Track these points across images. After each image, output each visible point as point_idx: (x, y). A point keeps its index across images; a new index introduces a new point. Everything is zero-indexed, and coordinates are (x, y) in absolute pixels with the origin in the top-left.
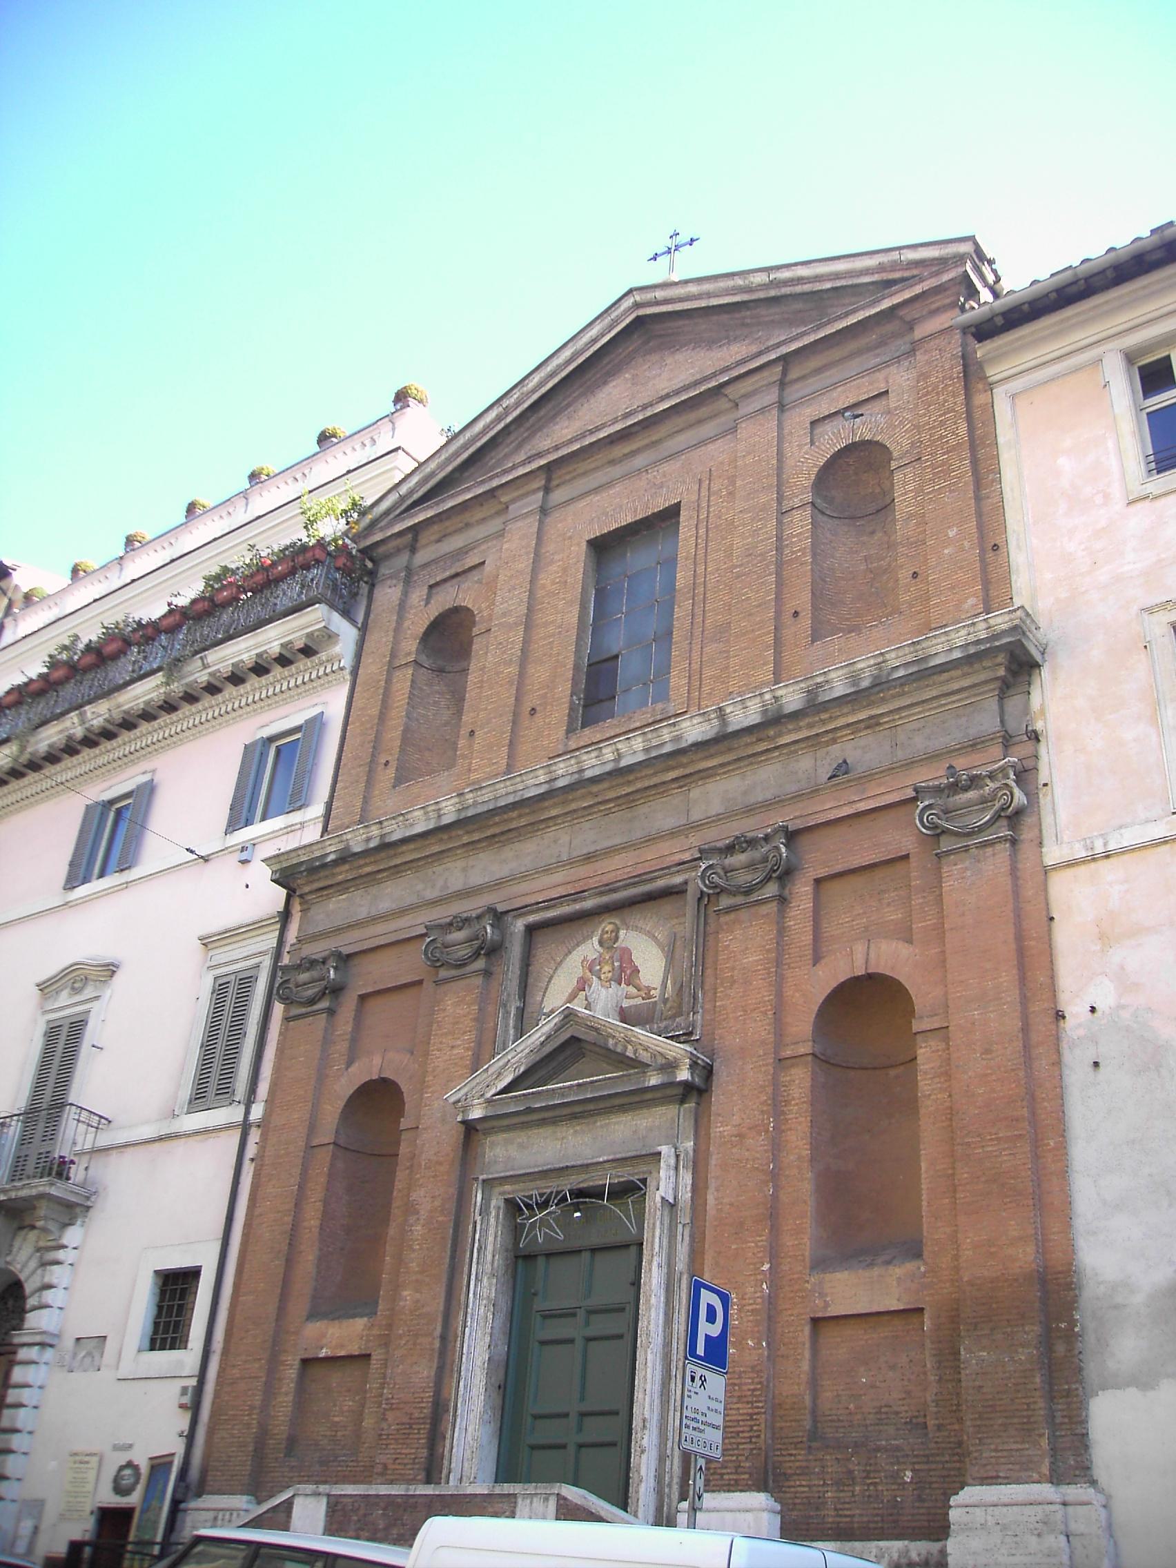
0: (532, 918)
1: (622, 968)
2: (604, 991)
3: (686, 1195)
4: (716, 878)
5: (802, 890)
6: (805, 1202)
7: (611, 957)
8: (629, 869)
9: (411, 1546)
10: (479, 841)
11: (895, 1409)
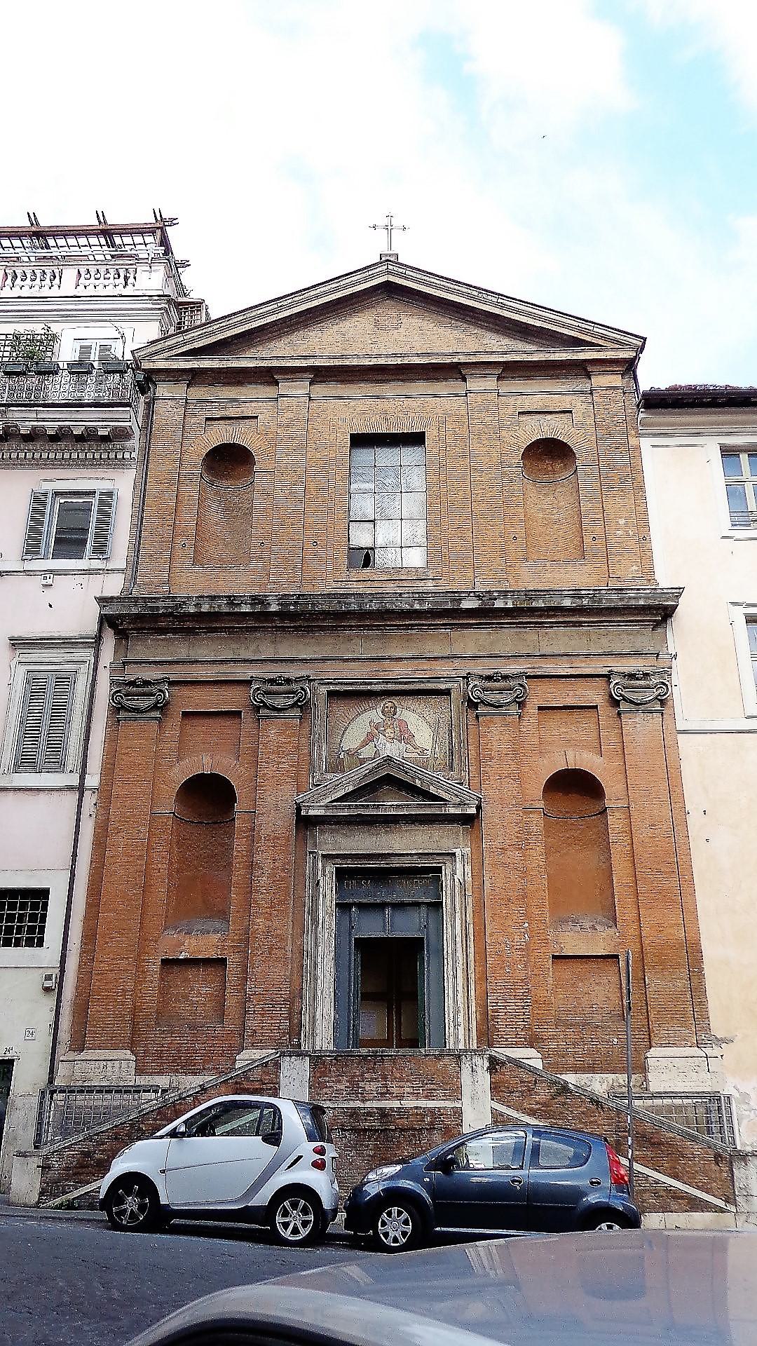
0: (332, 688)
9: (40, 943)
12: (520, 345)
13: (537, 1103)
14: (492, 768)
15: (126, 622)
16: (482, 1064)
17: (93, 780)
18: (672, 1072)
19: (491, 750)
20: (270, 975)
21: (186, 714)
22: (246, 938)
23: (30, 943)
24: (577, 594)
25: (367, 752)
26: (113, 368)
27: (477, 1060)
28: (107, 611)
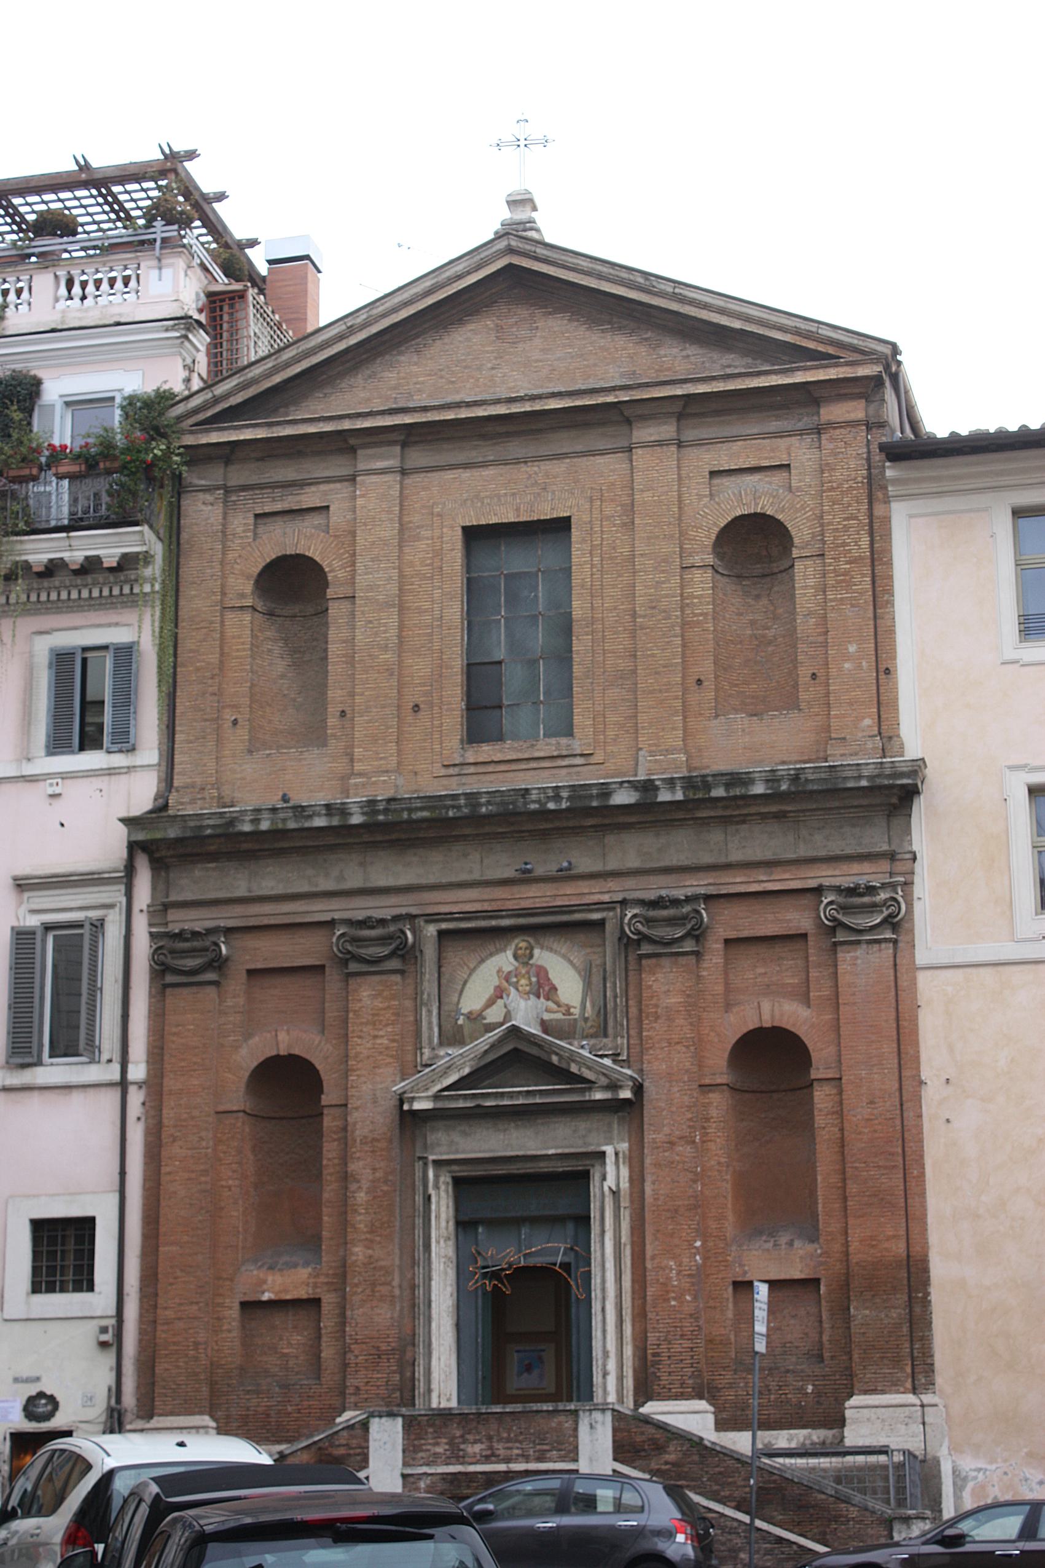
0: (444, 926)
1: (540, 985)
2: (522, 1003)
3: (625, 1185)
4: (639, 926)
5: (715, 945)
6: (725, 1197)
7: (528, 972)
8: (547, 899)
9: (91, 1288)
10: (381, 842)
11: (796, 1344)
13: (666, 1463)
14: (655, 1030)
15: (161, 844)
17: (137, 1071)
18: (876, 1421)
19: (656, 1006)
20: (374, 1317)
21: (251, 973)
22: (341, 1276)
23: (78, 1288)
25: (494, 1015)
28: (140, 836)
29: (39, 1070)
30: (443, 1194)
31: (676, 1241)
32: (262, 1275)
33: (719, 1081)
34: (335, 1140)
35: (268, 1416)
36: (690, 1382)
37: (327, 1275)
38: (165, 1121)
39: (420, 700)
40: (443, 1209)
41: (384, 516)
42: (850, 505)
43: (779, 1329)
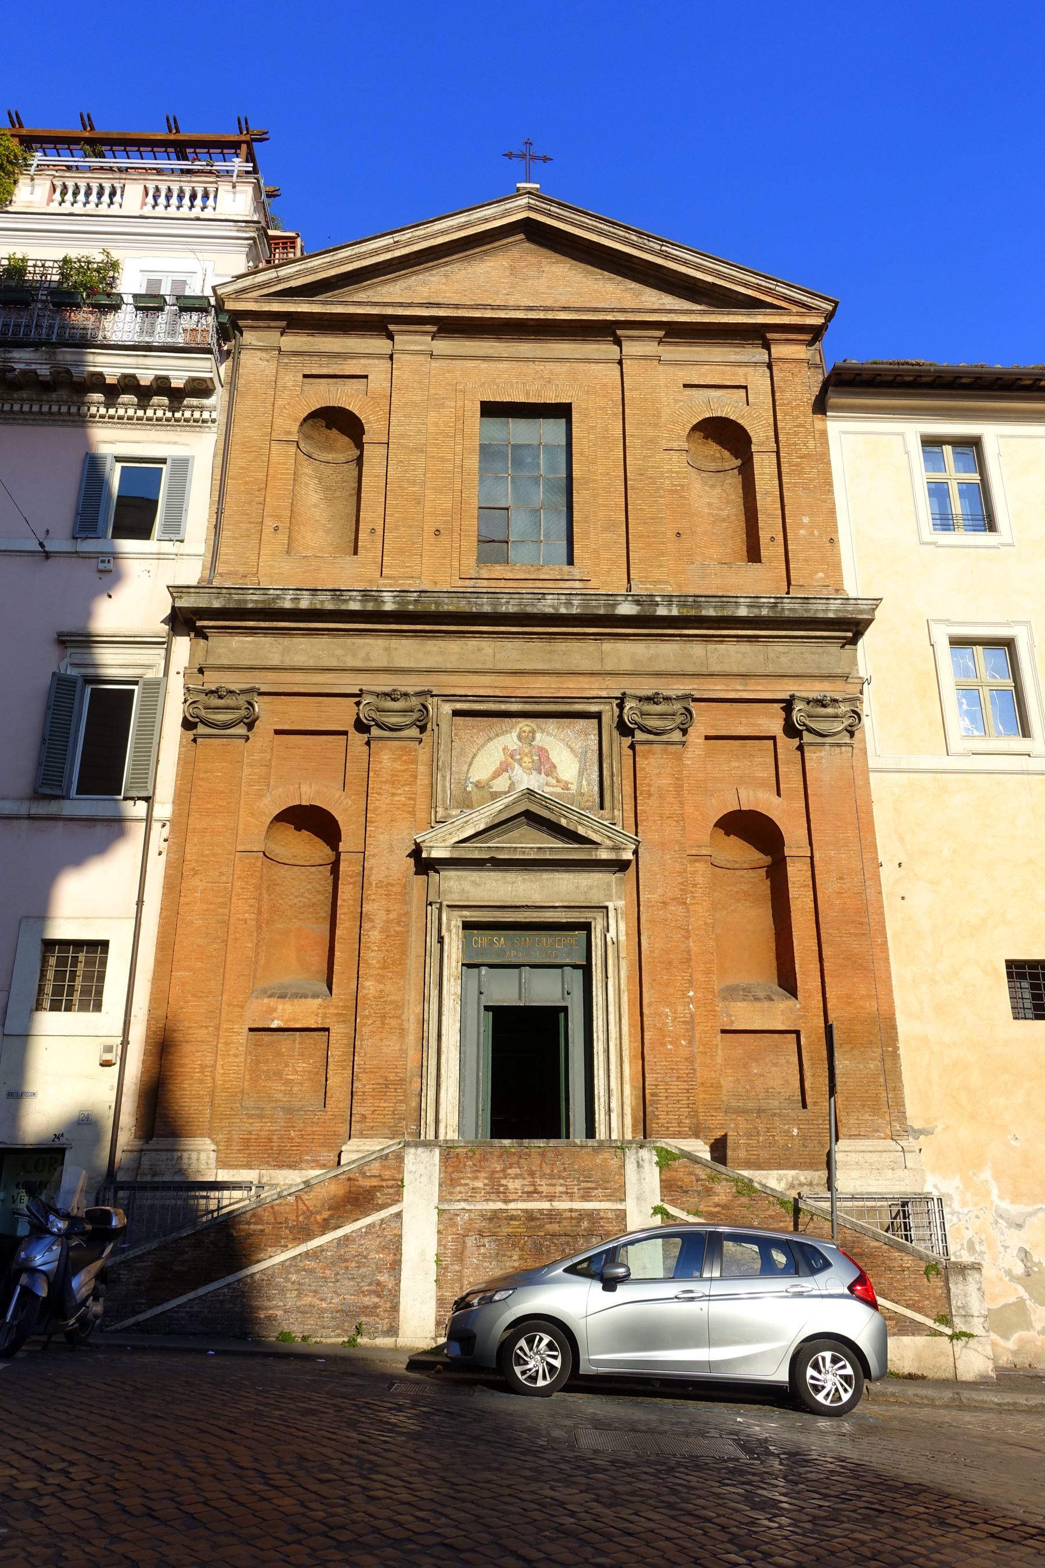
0: (459, 706)
6: (712, 953)
9: (98, 1007)
12: (687, 305)
13: (717, 1205)
16: (648, 1156)
18: (866, 1171)
19: (649, 785)
23: (84, 1007)
24: (755, 601)
26: (188, 305)
27: (644, 1153)
29: (67, 803)
30: (454, 936)
31: (671, 990)
32: (272, 1004)
33: (704, 852)
34: (350, 883)
35: (270, 1140)
36: (687, 1121)
37: (337, 1007)
38: (188, 857)
39: (441, 527)
40: (454, 950)
41: (415, 385)
42: (798, 417)
43: (762, 1075)
